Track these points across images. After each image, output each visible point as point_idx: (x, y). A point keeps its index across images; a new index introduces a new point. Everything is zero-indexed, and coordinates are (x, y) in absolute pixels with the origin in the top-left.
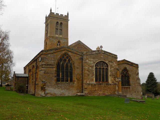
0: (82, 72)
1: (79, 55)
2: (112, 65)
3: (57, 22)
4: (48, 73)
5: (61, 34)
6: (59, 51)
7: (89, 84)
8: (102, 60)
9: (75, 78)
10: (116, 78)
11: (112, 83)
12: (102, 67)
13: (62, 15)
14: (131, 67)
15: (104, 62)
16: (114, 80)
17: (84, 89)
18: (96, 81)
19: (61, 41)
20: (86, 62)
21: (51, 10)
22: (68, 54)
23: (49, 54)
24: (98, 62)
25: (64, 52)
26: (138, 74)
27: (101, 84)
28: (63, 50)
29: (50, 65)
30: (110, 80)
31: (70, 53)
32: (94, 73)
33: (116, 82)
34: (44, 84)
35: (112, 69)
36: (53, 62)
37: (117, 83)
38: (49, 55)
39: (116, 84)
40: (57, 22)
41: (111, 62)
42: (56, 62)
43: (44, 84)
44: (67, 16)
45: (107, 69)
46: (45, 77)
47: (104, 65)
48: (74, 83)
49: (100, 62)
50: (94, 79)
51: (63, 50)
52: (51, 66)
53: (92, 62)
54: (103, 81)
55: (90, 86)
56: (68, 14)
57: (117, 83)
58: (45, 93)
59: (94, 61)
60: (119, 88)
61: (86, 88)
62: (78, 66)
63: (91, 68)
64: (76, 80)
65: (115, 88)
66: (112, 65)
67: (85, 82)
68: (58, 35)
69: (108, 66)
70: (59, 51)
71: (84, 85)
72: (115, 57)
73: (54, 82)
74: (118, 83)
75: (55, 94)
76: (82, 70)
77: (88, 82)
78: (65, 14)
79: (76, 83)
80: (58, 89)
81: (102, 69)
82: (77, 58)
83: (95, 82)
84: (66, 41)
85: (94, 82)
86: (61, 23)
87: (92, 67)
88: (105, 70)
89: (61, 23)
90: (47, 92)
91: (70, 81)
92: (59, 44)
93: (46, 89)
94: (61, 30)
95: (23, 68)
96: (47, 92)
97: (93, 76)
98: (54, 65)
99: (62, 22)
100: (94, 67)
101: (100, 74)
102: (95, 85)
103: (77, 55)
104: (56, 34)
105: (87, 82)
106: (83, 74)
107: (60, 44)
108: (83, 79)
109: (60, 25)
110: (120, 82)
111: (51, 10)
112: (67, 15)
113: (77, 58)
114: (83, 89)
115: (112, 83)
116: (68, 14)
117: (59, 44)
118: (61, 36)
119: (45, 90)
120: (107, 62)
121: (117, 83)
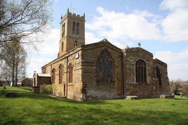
0: (123, 71)
1: (118, 53)
2: (149, 64)
3: (74, 23)
4: (88, 72)
5: (78, 34)
6: (99, 47)
7: (131, 85)
8: (142, 59)
9: (116, 78)
10: (154, 78)
11: (150, 82)
12: (141, 66)
13: (78, 16)
14: (162, 66)
15: (142, 60)
16: (151, 80)
17: (125, 90)
18: (137, 81)
19: (78, 41)
20: (127, 60)
21: (68, 10)
22: (107, 51)
23: (88, 50)
24: (137, 60)
25: (103, 48)
26: (167, 73)
27: (141, 84)
28: (103, 46)
29: (90, 63)
30: (148, 79)
31: (109, 50)
32: (135, 73)
33: (154, 81)
34: (85, 85)
35: (149, 68)
36: (93, 59)
37: (155, 83)
38: (89, 51)
39: (153, 84)
40: (74, 23)
41: (149, 60)
42: (96, 59)
43: (85, 85)
44: (83, 17)
45: (145, 68)
46: (85, 77)
47: (142, 63)
48: (114, 84)
49: (139, 60)
50: (135, 79)
51: (103, 46)
52: (91, 64)
53: (133, 61)
54: (142, 81)
55: (132, 87)
56: (84, 15)
57: (155, 83)
58: (86, 96)
59: (135, 59)
60: (157, 88)
61: (128, 89)
62: (118, 65)
63: (132, 67)
64: (116, 80)
65: (152, 88)
66: (149, 64)
67: (126, 82)
68: (75, 35)
69: (145, 65)
70: (99, 47)
71: (126, 85)
72: (151, 55)
73: (95, 83)
74: (156, 82)
75: (96, 97)
76: (123, 69)
77: (130, 82)
78: (81, 15)
79: (116, 83)
80: (100, 90)
81: (138, 67)
82: (117, 55)
83: (136, 82)
84: (83, 41)
85: (135, 82)
86: (78, 23)
87: (133, 65)
88: (143, 69)
89: (78, 23)
90: (88, 94)
91: (110, 82)
92: (76, 44)
93: (87, 91)
94: (78, 30)
95: (41, 69)
96: (88, 94)
97: (134, 76)
98: (94, 63)
99: (79, 22)
100: (135, 66)
101: (139, 73)
102: (136, 85)
103: (117, 52)
104: (73, 34)
105: (128, 82)
106: (124, 73)
107: (76, 44)
108: (123, 79)
109: (77, 25)
110: (158, 82)
111: (68, 10)
112: (83, 16)
113: (117, 55)
114: (124, 90)
115: (150, 82)
116: (84, 15)
117: (76, 44)
118: (78, 36)
119: (86, 92)
120: (145, 60)
121: (155, 82)
